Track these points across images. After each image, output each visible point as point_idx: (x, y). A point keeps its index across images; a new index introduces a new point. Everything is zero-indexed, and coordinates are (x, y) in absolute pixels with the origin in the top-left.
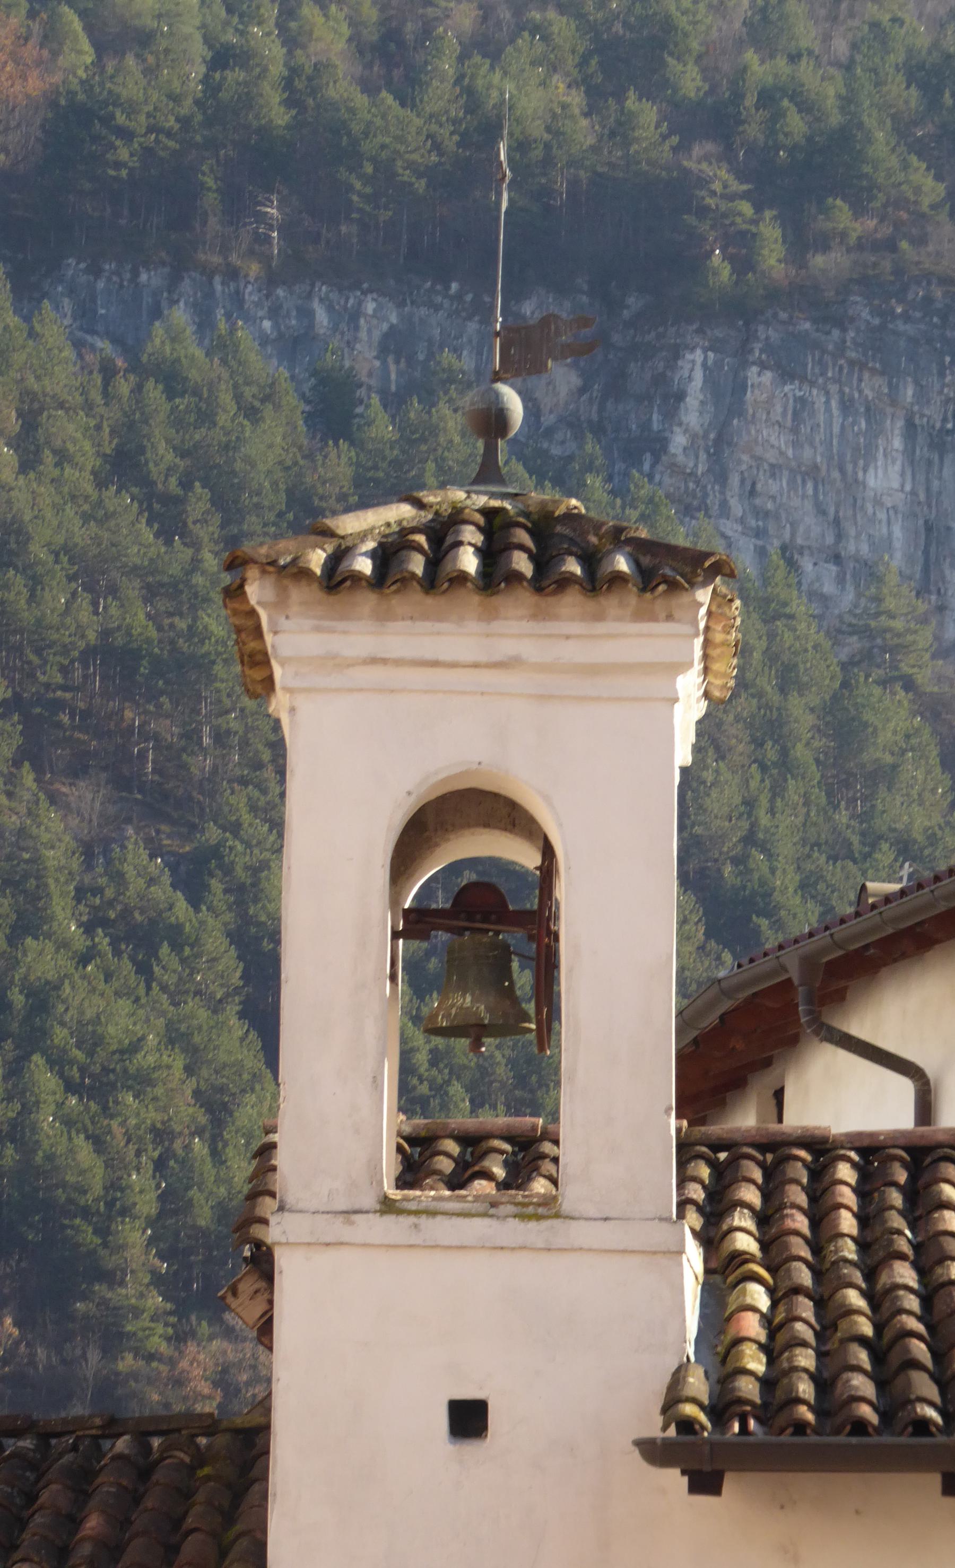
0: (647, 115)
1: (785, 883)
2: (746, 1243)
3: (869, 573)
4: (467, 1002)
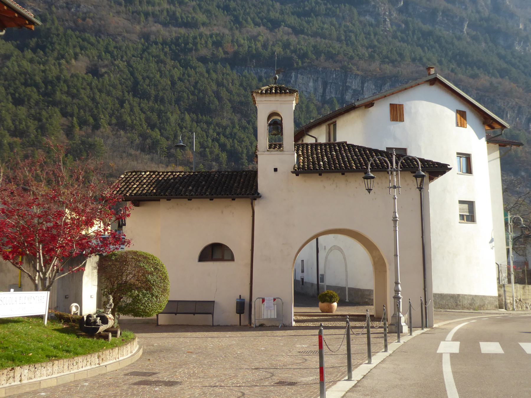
0: (288, 51)
1: (303, 122)
2: (300, 153)
3: (309, 93)
4: (274, 132)
